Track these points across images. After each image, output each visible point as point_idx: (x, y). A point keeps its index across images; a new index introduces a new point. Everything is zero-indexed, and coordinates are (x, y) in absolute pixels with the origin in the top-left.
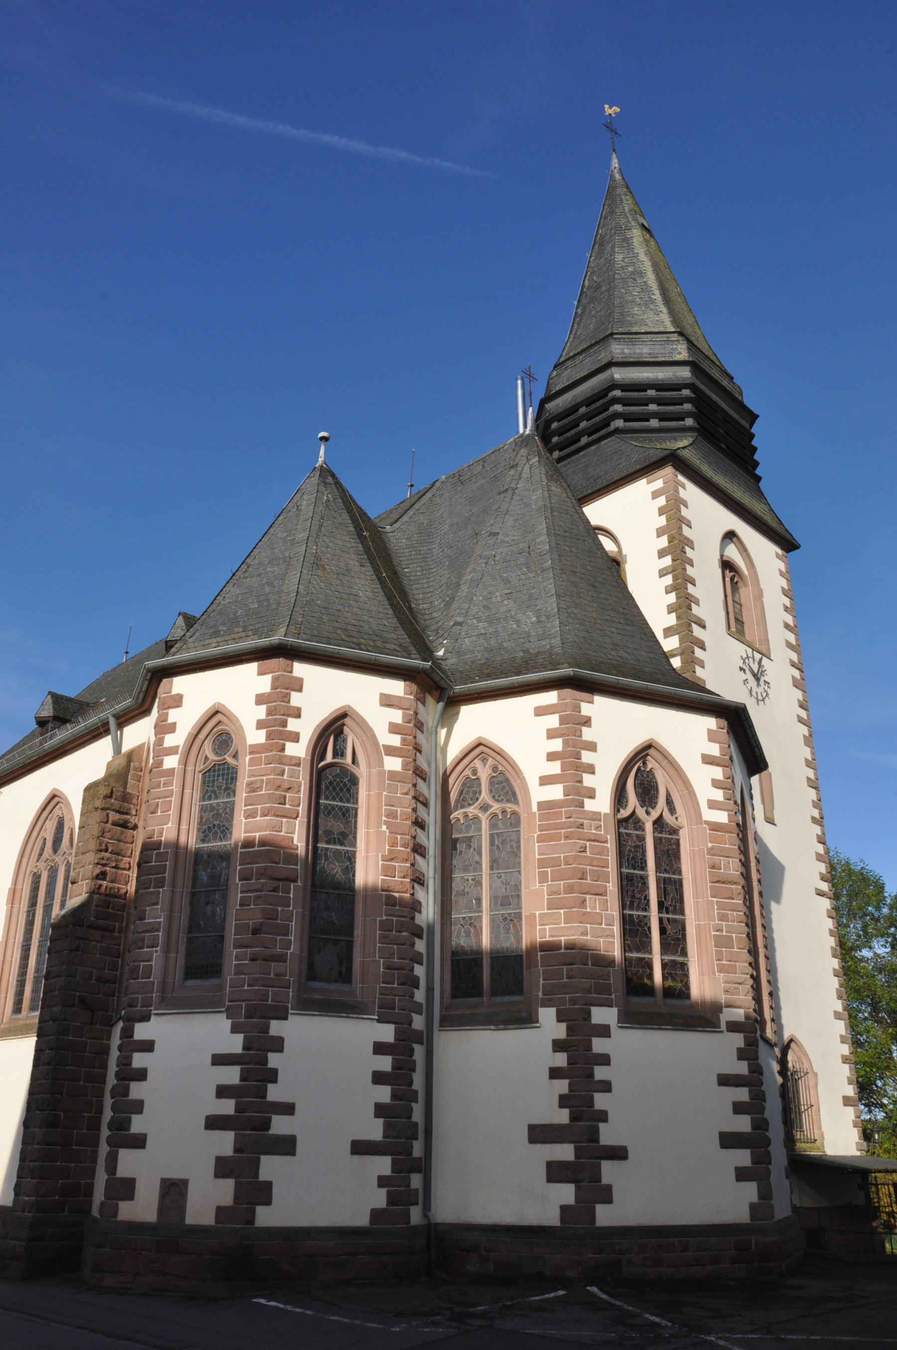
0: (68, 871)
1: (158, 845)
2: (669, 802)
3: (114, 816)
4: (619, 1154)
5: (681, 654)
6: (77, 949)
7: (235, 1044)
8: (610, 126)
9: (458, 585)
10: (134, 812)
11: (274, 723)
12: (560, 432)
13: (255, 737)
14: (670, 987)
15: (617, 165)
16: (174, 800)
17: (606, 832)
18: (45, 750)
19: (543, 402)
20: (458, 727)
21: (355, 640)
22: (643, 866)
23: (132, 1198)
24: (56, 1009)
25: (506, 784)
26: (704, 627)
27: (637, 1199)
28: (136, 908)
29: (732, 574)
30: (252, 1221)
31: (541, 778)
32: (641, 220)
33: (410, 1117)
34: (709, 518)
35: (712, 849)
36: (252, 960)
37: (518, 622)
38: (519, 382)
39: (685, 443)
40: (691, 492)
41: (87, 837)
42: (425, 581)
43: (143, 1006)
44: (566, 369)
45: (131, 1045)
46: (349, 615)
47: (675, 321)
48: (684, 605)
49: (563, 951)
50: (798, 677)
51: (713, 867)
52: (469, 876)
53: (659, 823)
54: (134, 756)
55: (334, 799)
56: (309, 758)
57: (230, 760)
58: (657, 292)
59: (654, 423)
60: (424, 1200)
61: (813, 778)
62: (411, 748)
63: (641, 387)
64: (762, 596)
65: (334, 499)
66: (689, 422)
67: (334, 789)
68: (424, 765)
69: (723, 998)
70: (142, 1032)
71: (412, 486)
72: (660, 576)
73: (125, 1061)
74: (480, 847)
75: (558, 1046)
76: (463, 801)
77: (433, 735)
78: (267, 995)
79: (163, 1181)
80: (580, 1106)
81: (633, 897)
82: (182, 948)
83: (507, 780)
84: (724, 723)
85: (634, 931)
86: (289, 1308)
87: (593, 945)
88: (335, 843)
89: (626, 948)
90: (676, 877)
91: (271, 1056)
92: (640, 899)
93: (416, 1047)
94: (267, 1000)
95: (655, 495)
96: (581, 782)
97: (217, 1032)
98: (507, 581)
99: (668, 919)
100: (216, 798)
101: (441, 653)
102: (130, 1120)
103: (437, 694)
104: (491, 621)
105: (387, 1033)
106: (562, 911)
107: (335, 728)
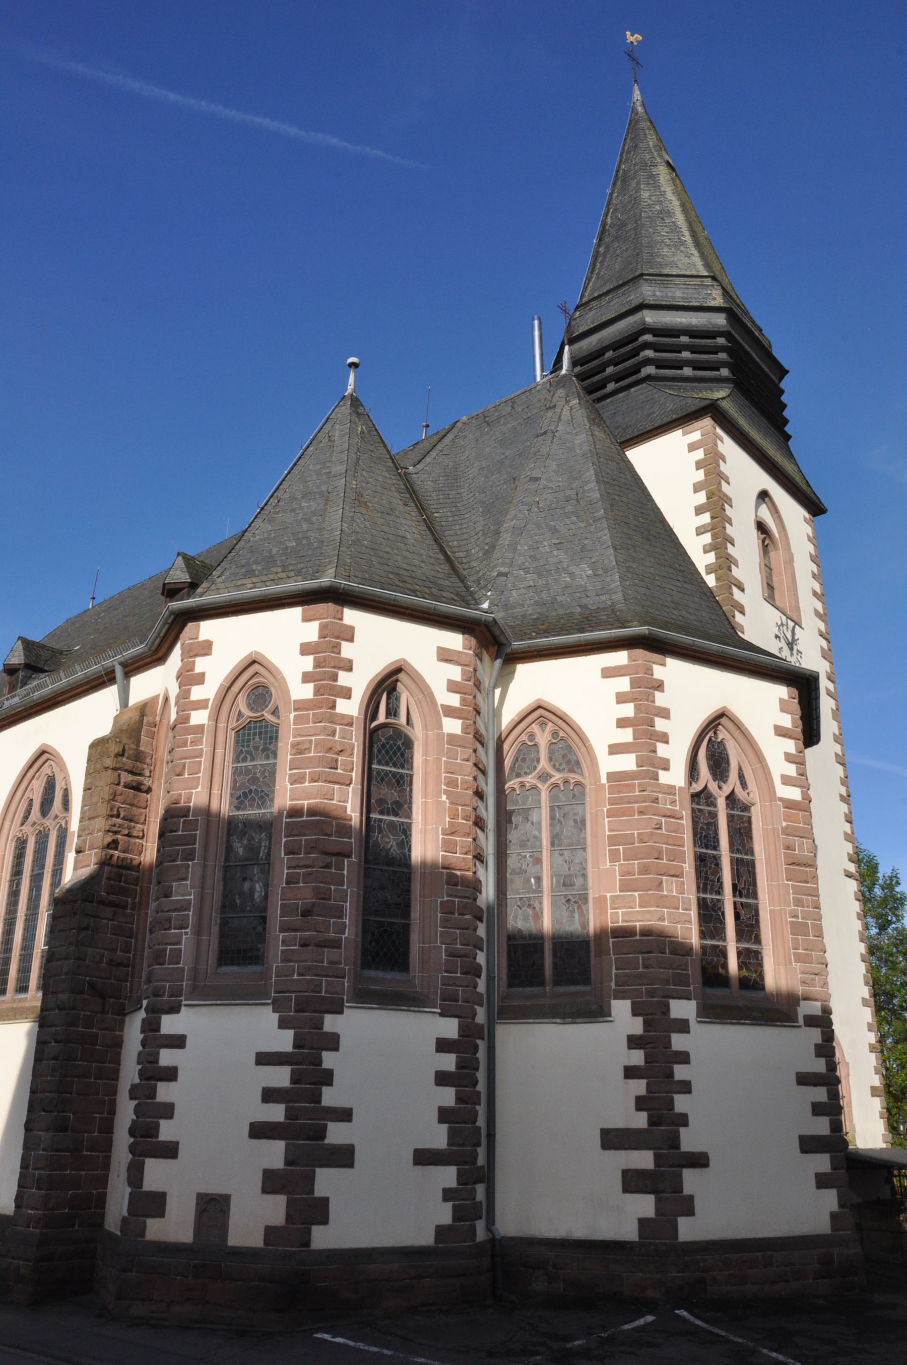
1: (185, 812)
2: (741, 777)
4: (700, 1161)
6: (86, 928)
7: (284, 1041)
8: (631, 54)
9: (498, 533)
10: (147, 773)
13: (306, 692)
14: (744, 977)
15: (639, 98)
16: (204, 761)
17: (682, 808)
18: (34, 701)
20: (513, 687)
21: (409, 586)
22: (716, 846)
24: (63, 997)
26: (743, 590)
28: (159, 883)
30: (307, 1243)
31: (610, 746)
32: (667, 157)
34: (745, 475)
35: (787, 828)
36: (304, 945)
37: (571, 575)
38: (536, 322)
40: (728, 446)
41: (95, 799)
42: (457, 527)
43: (171, 996)
44: (591, 310)
45: (154, 1039)
46: (398, 558)
47: (707, 266)
49: (638, 937)
50: (826, 648)
51: (788, 848)
53: (731, 799)
54: (148, 710)
55: (387, 764)
56: (362, 717)
57: (269, 717)
58: (687, 234)
59: (687, 371)
60: (488, 1212)
61: (840, 754)
62: (471, 709)
63: (674, 332)
64: (793, 561)
65: (369, 431)
66: (725, 372)
67: (387, 752)
68: (483, 731)
69: (800, 990)
70: (170, 1024)
71: (427, 426)
72: (698, 535)
73: (151, 1059)
74: (540, 823)
75: (634, 1042)
78: (321, 985)
79: (200, 1196)
80: (660, 1109)
81: (707, 878)
82: (215, 930)
83: (569, 748)
84: (795, 692)
85: (710, 916)
86: (361, 1345)
87: (671, 932)
88: (388, 814)
89: (703, 935)
90: (749, 857)
91: (325, 1054)
92: (713, 881)
93: (479, 1041)
94: (321, 992)
95: (692, 447)
96: (655, 751)
97: (261, 1027)
98: (554, 531)
99: (742, 903)
100: (253, 759)
102: (157, 1126)
103: (493, 649)
104: (540, 572)
105: (450, 1028)
106: (636, 894)
107: (388, 684)
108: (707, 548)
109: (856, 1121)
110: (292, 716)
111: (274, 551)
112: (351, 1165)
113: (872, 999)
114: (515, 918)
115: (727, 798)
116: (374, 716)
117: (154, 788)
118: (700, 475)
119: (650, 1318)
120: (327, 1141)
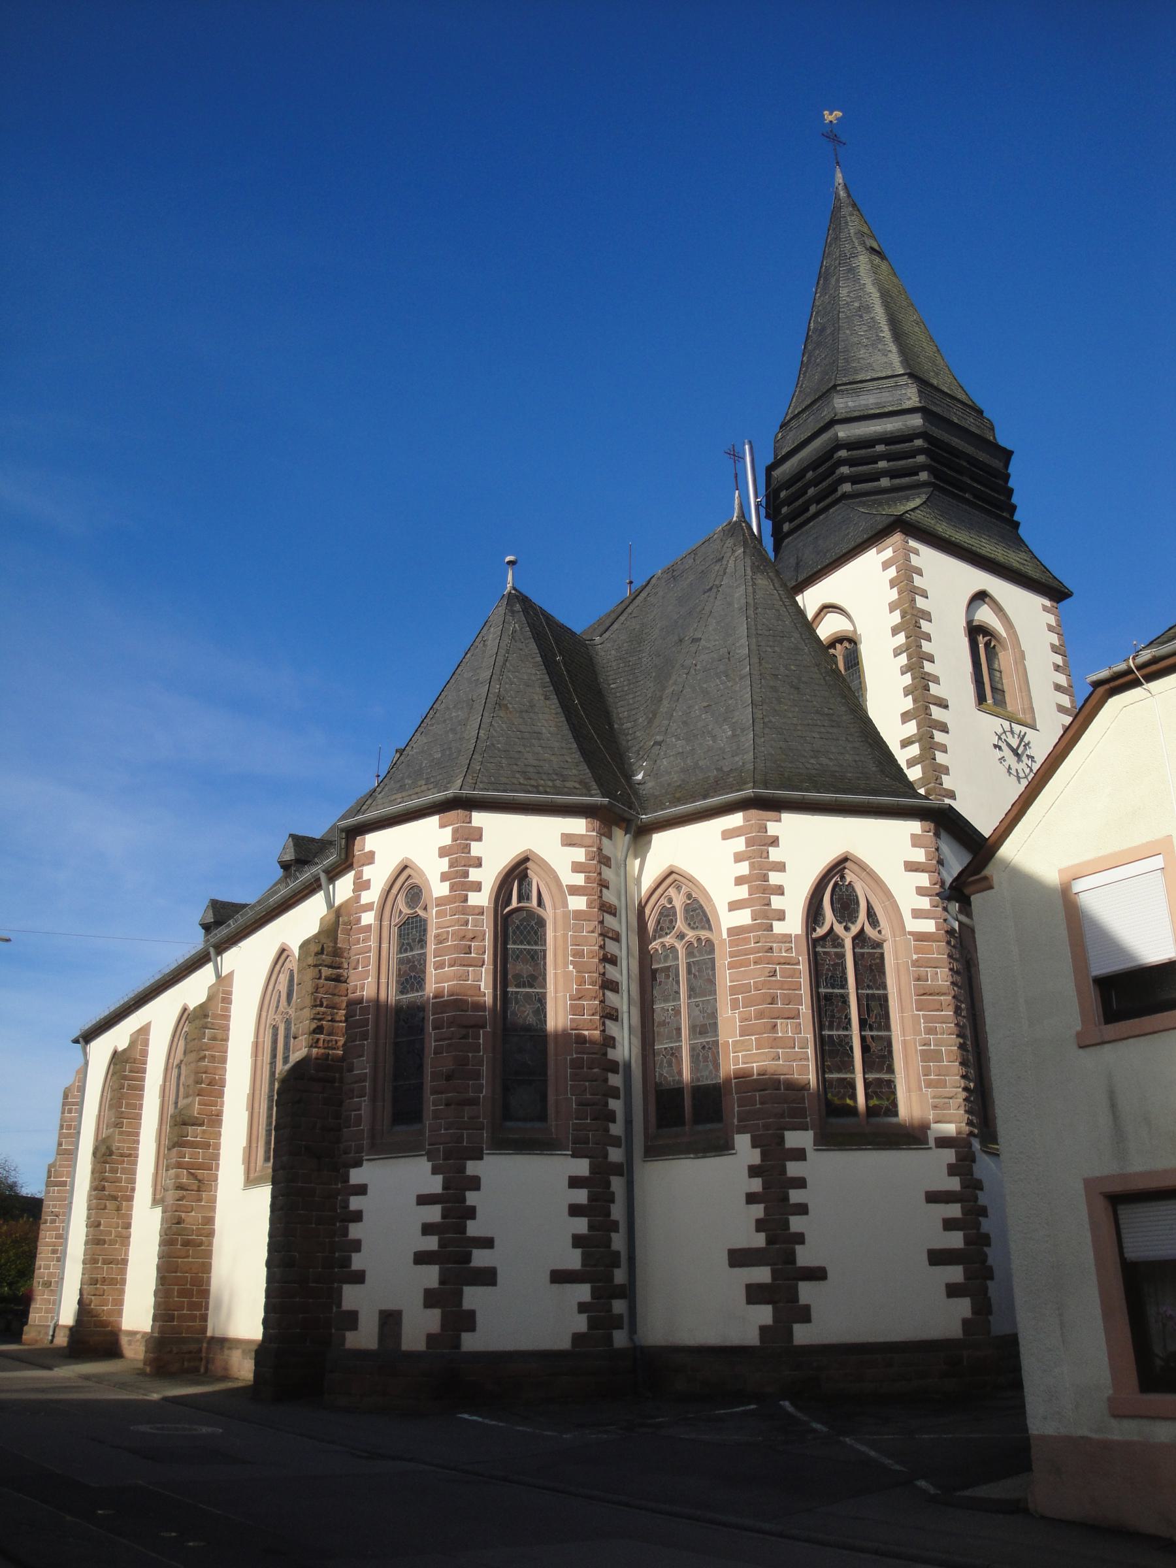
0: (288, 1029)
1: (360, 1001)
3: (326, 972)
4: (818, 1274)
5: (919, 741)
7: (435, 1185)
8: (832, 136)
10: (346, 966)
11: (457, 874)
12: (789, 501)
14: (875, 1106)
16: (373, 955)
19: (770, 469)
20: (650, 856)
21: (533, 782)
22: (843, 984)
23: (356, 1328)
25: (699, 914)
27: (836, 1316)
29: (986, 639)
33: (609, 1246)
34: (948, 580)
35: (917, 961)
37: (714, 738)
38: (747, 447)
39: (918, 502)
40: (927, 557)
44: (791, 430)
48: (921, 686)
51: (918, 979)
52: (669, 1005)
53: (860, 938)
54: (343, 911)
55: (522, 943)
57: (421, 913)
58: (886, 328)
59: (885, 482)
66: (924, 476)
67: (521, 933)
70: (356, 1176)
71: (631, 583)
75: (754, 1171)
76: (661, 931)
77: (622, 869)
79: (381, 1312)
81: (833, 1016)
83: (701, 907)
84: (930, 825)
85: (831, 1052)
88: (524, 986)
89: (822, 1068)
92: (840, 1018)
95: (886, 565)
96: (769, 904)
99: (872, 1037)
100: (412, 950)
101: (640, 777)
103: (624, 825)
105: (582, 1167)
107: (518, 873)
114: (661, 1067)
115: (854, 939)
119: (825, 1429)
120: (472, 1264)
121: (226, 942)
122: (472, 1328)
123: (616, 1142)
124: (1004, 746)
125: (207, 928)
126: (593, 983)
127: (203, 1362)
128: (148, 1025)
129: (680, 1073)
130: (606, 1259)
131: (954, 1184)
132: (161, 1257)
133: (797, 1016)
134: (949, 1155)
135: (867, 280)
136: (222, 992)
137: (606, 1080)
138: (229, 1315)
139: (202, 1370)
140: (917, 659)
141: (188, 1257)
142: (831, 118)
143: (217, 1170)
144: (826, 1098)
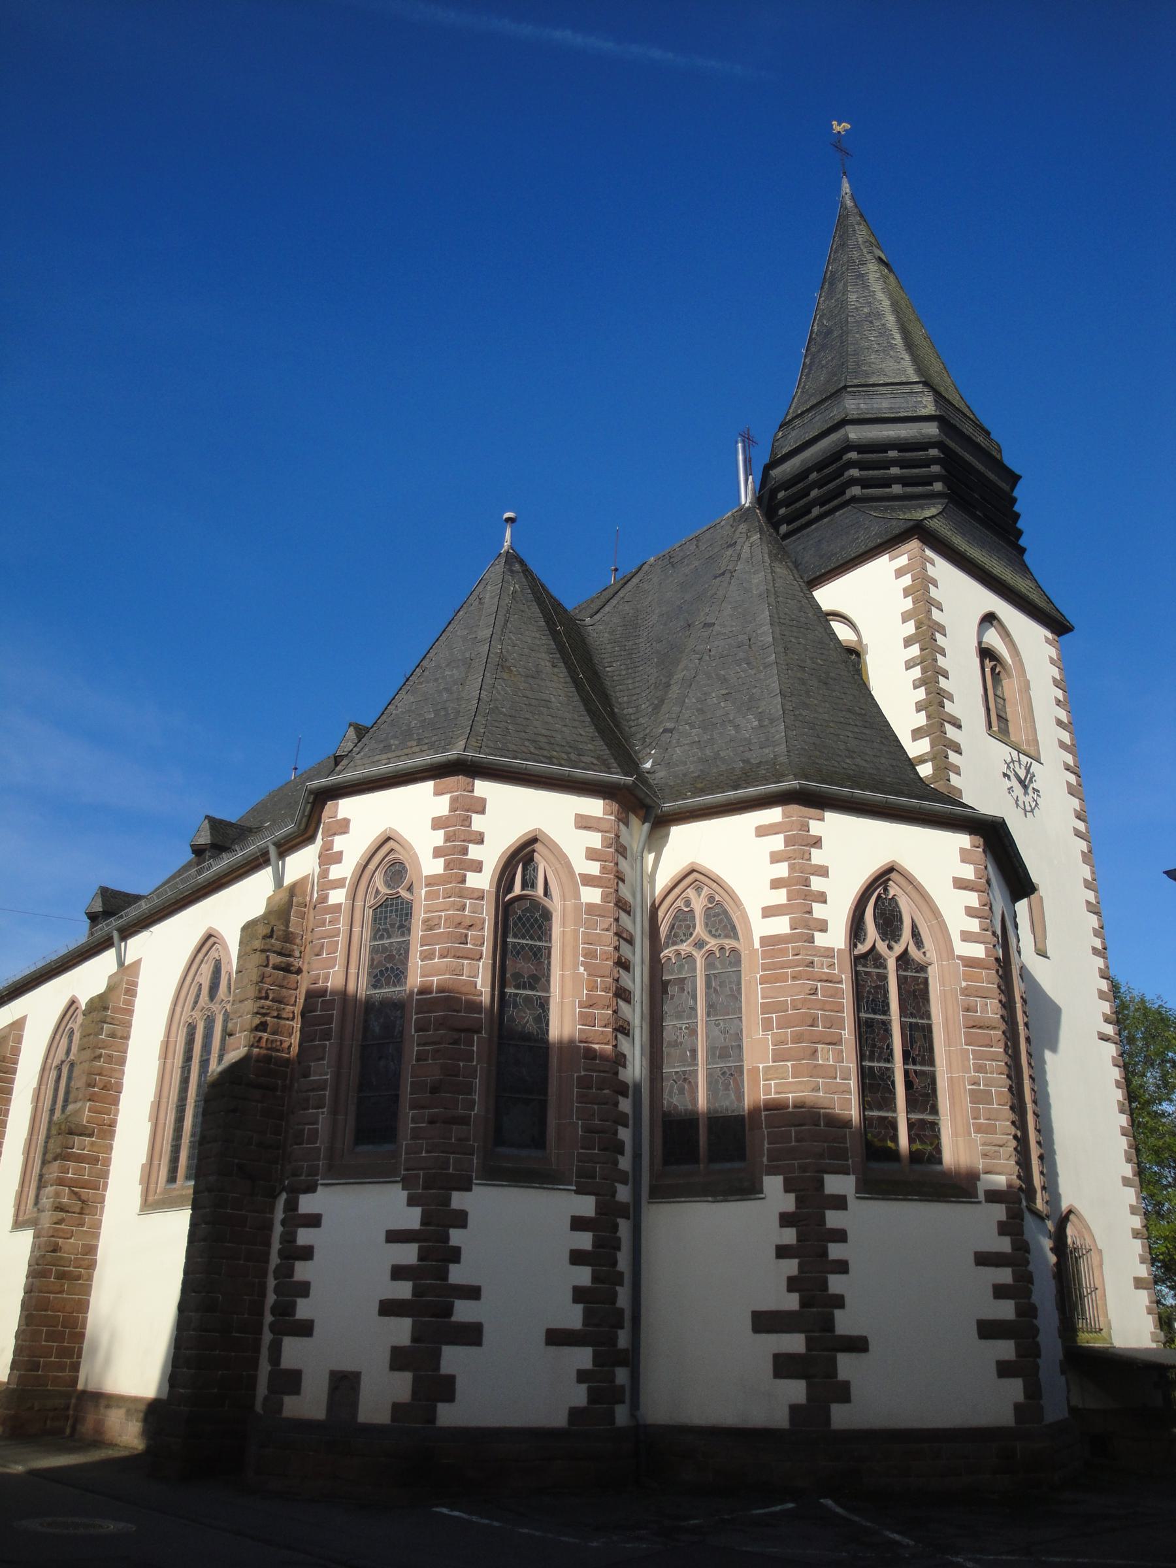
1: (323, 992)
2: (916, 934)
3: (275, 959)
4: (858, 1345)
5: (933, 760)
7: (412, 1219)
8: (838, 143)
9: (668, 685)
10: (297, 954)
12: (787, 503)
14: (918, 1150)
16: (341, 940)
17: (840, 971)
19: (768, 468)
20: (667, 851)
21: (545, 753)
22: (886, 1010)
25: (723, 919)
26: (959, 727)
31: (764, 909)
33: (614, 1303)
34: (962, 597)
35: (966, 988)
37: (737, 727)
39: (933, 511)
40: (941, 569)
44: (793, 429)
47: (919, 370)
48: (935, 702)
51: (968, 1010)
52: (683, 1023)
53: (904, 959)
54: (298, 891)
55: (523, 937)
57: (404, 894)
58: (898, 336)
59: (897, 489)
62: (612, 876)
63: (881, 447)
66: (938, 486)
67: (524, 925)
69: (980, 1164)
70: (307, 1204)
75: (786, 1220)
76: (675, 937)
79: (333, 1374)
81: (874, 1046)
83: (725, 912)
84: (979, 840)
85: (874, 1086)
86: (474, 1518)
88: (524, 988)
89: (864, 1105)
91: (452, 1231)
95: (899, 573)
96: (810, 912)
99: (915, 1071)
100: (389, 937)
101: (648, 765)
105: (586, 1206)
106: (789, 1064)
107: (523, 855)
108: (917, 683)
109: (1113, 1314)
110: (423, 892)
111: (413, 725)
112: (478, 1343)
113: (1137, 1178)
114: (671, 1093)
115: (898, 959)
116: (510, 888)
117: (305, 968)
118: (908, 603)
119: (791, 1505)
120: (453, 1319)
121: (135, 925)
122: (450, 1397)
123: (623, 1178)
124: (1012, 777)
125: (93, 918)
126: (606, 990)
127: (70, 1423)
128: (24, 1019)
129: (694, 1100)
130: (609, 1318)
131: (1004, 1245)
132: (28, 1291)
133: (837, 1043)
134: (999, 1212)
135: (877, 288)
136: (125, 983)
137: (616, 1104)
138: (108, 1361)
139: (68, 1431)
140: (931, 675)
141: (61, 1292)
142: (839, 128)
143: (105, 1189)
144: (866, 1139)
